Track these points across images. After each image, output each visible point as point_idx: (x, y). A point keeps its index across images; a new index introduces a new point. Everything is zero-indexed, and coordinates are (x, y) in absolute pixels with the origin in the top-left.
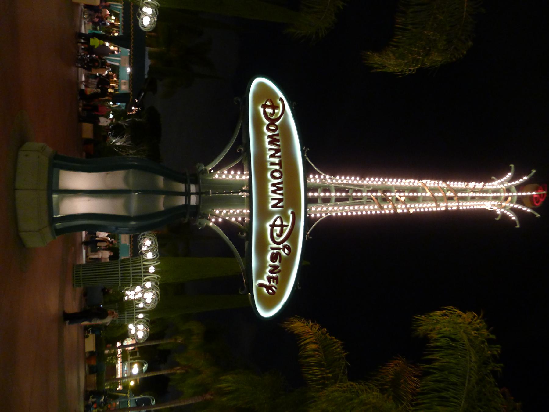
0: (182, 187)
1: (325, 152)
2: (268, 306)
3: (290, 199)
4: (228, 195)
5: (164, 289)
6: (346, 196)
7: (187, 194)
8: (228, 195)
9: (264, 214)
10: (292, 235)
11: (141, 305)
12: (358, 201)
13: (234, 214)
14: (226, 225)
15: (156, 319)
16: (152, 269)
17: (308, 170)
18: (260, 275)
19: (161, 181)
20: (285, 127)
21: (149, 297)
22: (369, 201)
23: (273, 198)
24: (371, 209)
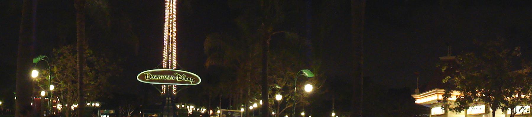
0: (167, 101)
1: (155, 61)
2: (198, 80)
3: (171, 73)
4: (169, 89)
5: (189, 103)
6: (170, 53)
7: (168, 100)
8: (169, 89)
9: (175, 81)
10: (182, 74)
11: (211, 112)
12: (172, 51)
13: (174, 89)
14: (176, 91)
15: (198, 105)
16: (183, 106)
17: (161, 67)
18: (190, 83)
19: (166, 107)
20: (152, 73)
21: (192, 107)
22: (172, 46)
23: (172, 78)
24: (175, 45)
